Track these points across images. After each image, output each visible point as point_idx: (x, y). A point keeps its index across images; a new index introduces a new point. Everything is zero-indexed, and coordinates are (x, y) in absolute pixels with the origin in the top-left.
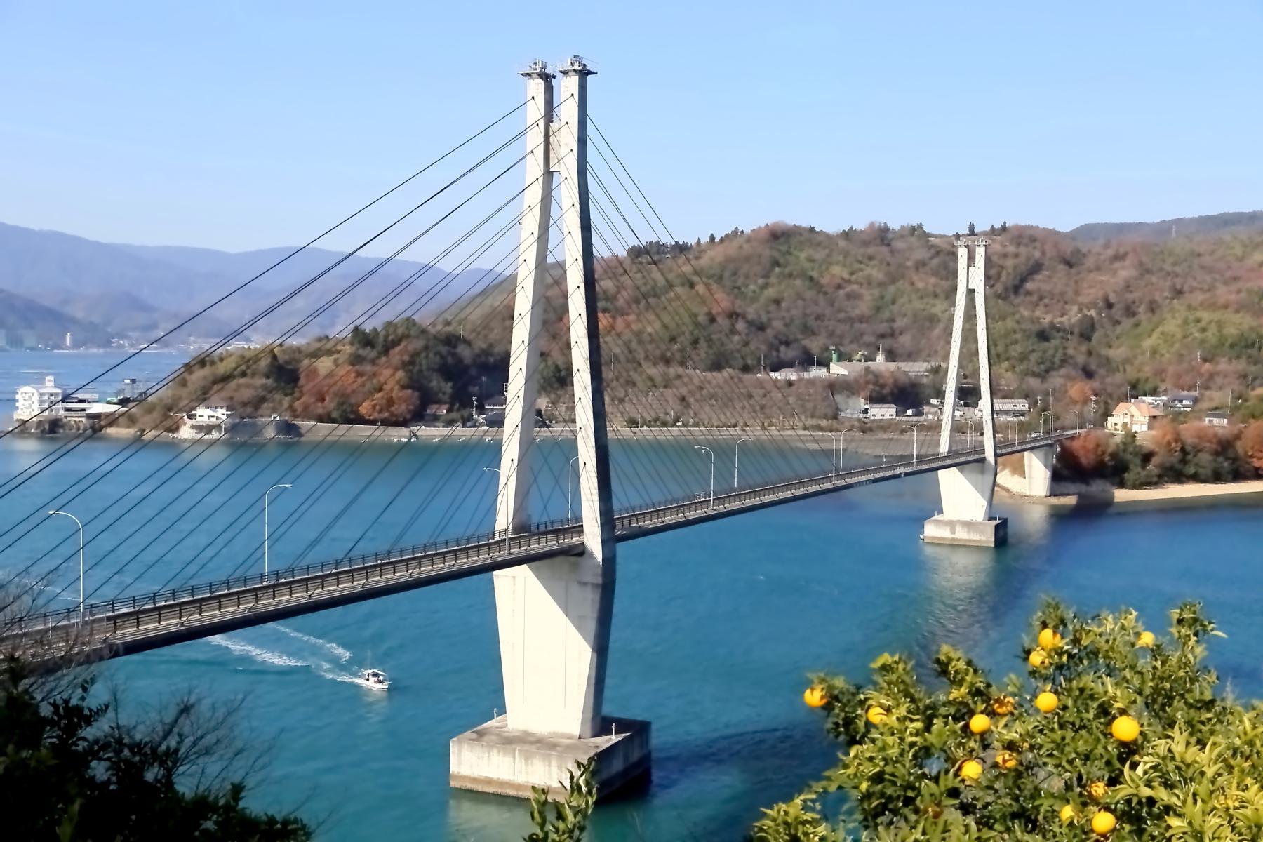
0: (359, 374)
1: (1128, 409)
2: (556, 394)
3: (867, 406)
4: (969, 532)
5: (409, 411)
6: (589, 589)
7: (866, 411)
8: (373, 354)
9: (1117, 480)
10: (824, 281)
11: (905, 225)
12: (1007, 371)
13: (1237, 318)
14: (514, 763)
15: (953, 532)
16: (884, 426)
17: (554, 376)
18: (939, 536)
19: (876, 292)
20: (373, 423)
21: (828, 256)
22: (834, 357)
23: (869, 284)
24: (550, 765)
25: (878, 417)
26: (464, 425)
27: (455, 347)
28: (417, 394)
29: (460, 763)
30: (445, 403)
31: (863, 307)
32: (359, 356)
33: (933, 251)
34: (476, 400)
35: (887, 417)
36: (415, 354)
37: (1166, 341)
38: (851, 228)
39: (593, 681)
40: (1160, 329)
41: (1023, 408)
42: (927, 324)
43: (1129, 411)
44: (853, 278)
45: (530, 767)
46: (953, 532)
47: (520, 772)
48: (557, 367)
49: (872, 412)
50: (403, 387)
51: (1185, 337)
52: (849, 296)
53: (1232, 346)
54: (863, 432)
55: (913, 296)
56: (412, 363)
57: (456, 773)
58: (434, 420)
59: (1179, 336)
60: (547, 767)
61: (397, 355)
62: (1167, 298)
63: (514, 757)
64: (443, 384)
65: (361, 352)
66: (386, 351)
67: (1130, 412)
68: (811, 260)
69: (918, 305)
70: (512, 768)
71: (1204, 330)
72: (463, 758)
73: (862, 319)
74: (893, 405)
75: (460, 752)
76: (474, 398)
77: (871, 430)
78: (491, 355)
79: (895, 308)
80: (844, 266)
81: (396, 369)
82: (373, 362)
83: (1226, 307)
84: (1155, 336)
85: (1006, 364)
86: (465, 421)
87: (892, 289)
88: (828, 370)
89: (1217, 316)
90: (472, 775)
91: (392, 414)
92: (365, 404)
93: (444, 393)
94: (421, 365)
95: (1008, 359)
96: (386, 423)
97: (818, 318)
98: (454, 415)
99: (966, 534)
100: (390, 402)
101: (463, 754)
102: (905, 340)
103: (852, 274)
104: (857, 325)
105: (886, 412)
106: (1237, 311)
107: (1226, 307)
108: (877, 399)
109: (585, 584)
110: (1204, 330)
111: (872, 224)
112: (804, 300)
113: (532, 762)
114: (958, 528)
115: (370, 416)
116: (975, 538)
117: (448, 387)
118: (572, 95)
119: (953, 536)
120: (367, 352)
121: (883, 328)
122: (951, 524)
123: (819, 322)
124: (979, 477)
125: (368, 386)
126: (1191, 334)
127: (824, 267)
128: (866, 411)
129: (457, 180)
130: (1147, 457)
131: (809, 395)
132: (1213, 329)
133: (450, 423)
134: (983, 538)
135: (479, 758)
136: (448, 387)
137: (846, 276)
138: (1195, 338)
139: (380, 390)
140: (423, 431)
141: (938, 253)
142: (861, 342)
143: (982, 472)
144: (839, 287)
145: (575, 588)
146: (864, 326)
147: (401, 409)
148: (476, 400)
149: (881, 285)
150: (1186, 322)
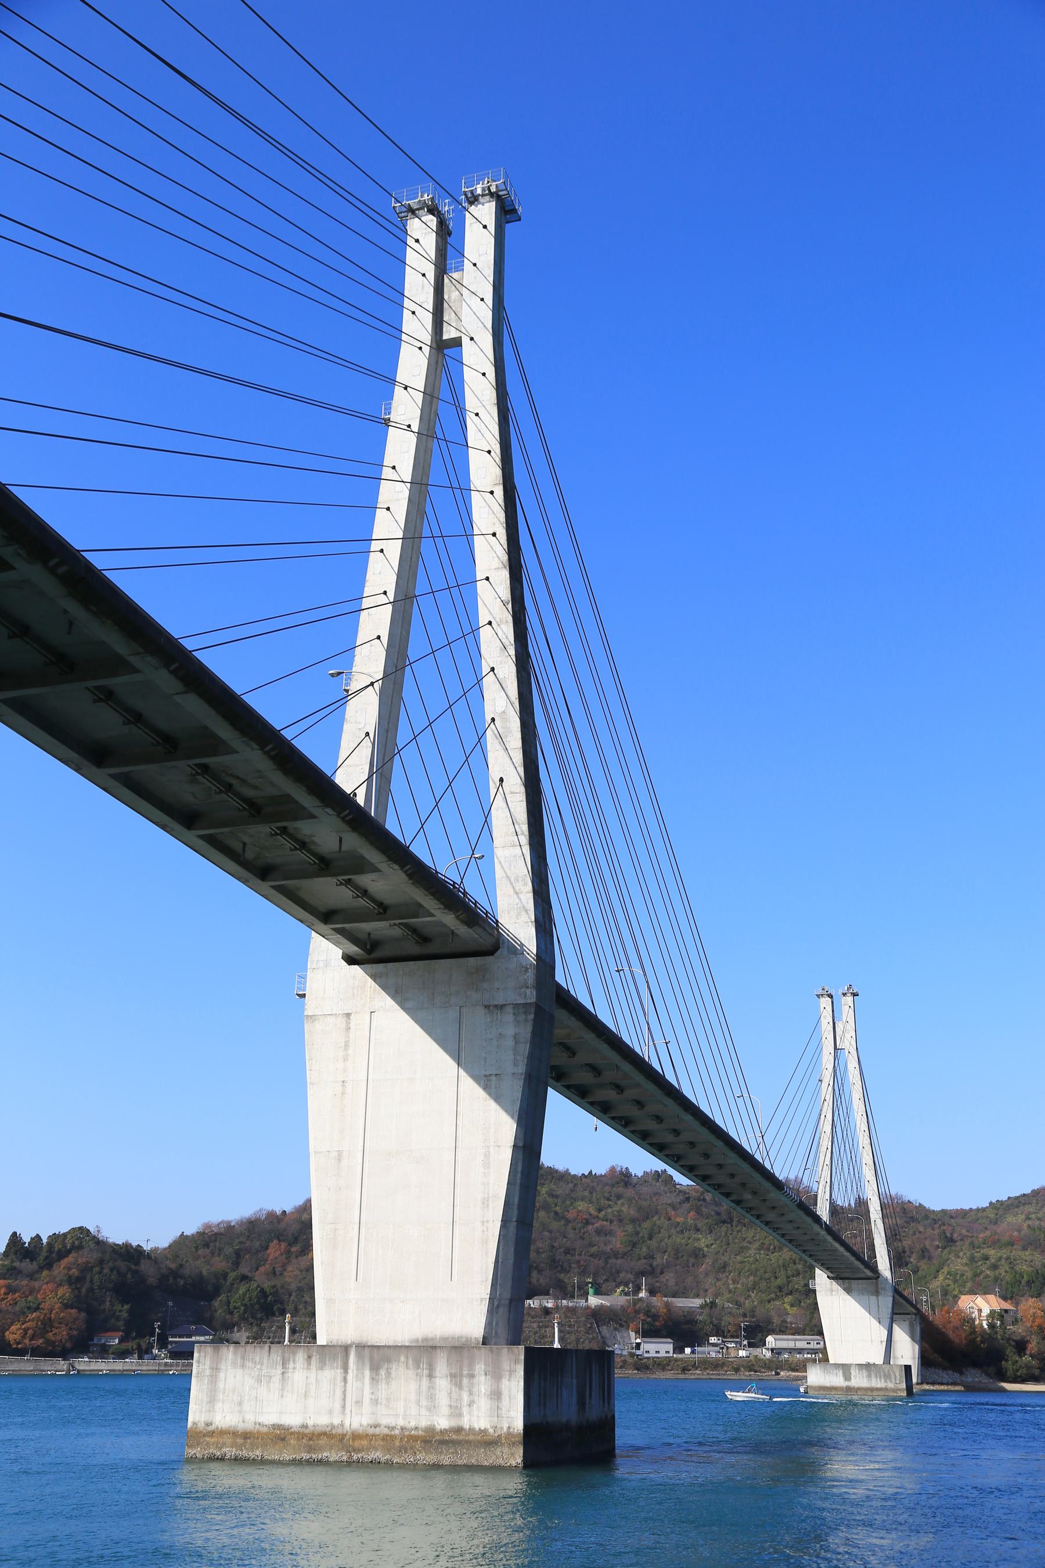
0: (10, 1290)
1: (974, 1302)
2: (258, 1325)
3: (638, 1341)
4: (869, 1376)
5: (71, 1337)
6: (509, 1017)
7: (638, 1346)
8: (34, 1266)
9: (992, 1370)
10: (570, 1216)
11: (648, 1170)
12: (792, 1306)
13: (1027, 1255)
14: (345, 1380)
15: (847, 1377)
16: (661, 1364)
17: (258, 1302)
18: (828, 1385)
19: (630, 1228)
20: (20, 1352)
21: (572, 1191)
22: (591, 1291)
23: (620, 1221)
24: (431, 1376)
25: (653, 1354)
26: (140, 1357)
27: (137, 1264)
28: (83, 1315)
29: (212, 1400)
30: (118, 1330)
31: (618, 1241)
32: (15, 1268)
33: (681, 1197)
34: (159, 1327)
35: (662, 1354)
36: (86, 1269)
37: (955, 1281)
38: (591, 1172)
39: (514, 1214)
40: (946, 1270)
41: (818, 1346)
42: (692, 1260)
43: (975, 1304)
44: (602, 1215)
45: (383, 1385)
46: (847, 1377)
47: (359, 1403)
48: (262, 1291)
49: (645, 1347)
50: (66, 1306)
51: (976, 1275)
52: (599, 1232)
53: (1029, 1283)
54: (638, 1370)
55: (673, 1231)
56: (80, 1279)
57: (201, 1426)
58: (103, 1352)
59: (969, 1274)
60: (425, 1382)
61: (60, 1269)
62: (938, 1247)
63: (345, 1368)
64: (118, 1307)
65: (17, 1264)
66: (49, 1265)
67: (977, 1306)
68: (551, 1194)
69: (678, 1239)
70: (339, 1393)
71: (995, 1267)
72: (221, 1385)
73: (616, 1255)
74: (670, 1340)
75: (215, 1369)
76: (157, 1324)
77: (647, 1368)
78: (182, 1277)
79: (654, 1243)
80: (591, 1202)
81: (60, 1285)
82: (31, 1276)
83: (1011, 1244)
84: (941, 1277)
85: (789, 1299)
86: (143, 1352)
87: (646, 1225)
88: (587, 1300)
89: (1004, 1253)
90: (241, 1427)
91: (48, 1342)
92: (13, 1328)
93: (118, 1319)
94: (92, 1281)
95: (791, 1293)
96: (37, 1352)
97: (567, 1252)
98: (131, 1345)
99: (865, 1380)
100: (47, 1324)
101: (222, 1375)
102: (669, 1278)
103: (600, 1210)
104: (612, 1261)
105: (660, 1348)
106: (1025, 1249)
107: (1011, 1244)
108: (650, 1333)
109: (501, 1007)
110: (995, 1267)
111: (613, 1169)
112: (550, 1232)
113: (388, 1373)
114: (854, 1372)
115: (18, 1343)
116: (879, 1386)
117: (123, 1310)
118: (367, 734)
119: (847, 1384)
120: (27, 1266)
121: (642, 1264)
122: (845, 1369)
123: (569, 1257)
124: (873, 1298)
125: (22, 1303)
126: (982, 1272)
127: (568, 1202)
128: (638, 1346)
129: (354, 106)
130: (1021, 1346)
131: (570, 1326)
132: (1004, 1267)
133: (122, 1354)
134: (890, 1385)
135: (259, 1380)
136: (123, 1310)
137: (594, 1212)
138: (987, 1276)
139: (37, 1309)
140: (84, 1364)
141: (688, 1199)
142: (618, 1280)
143: (877, 1293)
144: (587, 1223)
145: (478, 1018)
146: (619, 1262)
147: (60, 1334)
148: (159, 1327)
149: (633, 1221)
150: (972, 1259)
